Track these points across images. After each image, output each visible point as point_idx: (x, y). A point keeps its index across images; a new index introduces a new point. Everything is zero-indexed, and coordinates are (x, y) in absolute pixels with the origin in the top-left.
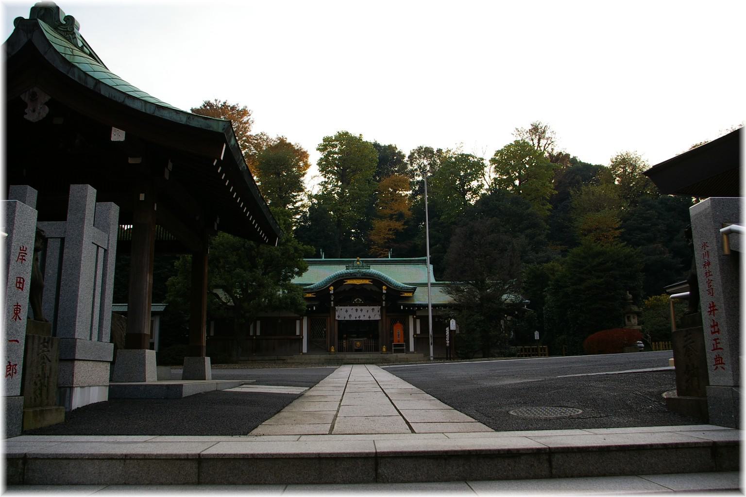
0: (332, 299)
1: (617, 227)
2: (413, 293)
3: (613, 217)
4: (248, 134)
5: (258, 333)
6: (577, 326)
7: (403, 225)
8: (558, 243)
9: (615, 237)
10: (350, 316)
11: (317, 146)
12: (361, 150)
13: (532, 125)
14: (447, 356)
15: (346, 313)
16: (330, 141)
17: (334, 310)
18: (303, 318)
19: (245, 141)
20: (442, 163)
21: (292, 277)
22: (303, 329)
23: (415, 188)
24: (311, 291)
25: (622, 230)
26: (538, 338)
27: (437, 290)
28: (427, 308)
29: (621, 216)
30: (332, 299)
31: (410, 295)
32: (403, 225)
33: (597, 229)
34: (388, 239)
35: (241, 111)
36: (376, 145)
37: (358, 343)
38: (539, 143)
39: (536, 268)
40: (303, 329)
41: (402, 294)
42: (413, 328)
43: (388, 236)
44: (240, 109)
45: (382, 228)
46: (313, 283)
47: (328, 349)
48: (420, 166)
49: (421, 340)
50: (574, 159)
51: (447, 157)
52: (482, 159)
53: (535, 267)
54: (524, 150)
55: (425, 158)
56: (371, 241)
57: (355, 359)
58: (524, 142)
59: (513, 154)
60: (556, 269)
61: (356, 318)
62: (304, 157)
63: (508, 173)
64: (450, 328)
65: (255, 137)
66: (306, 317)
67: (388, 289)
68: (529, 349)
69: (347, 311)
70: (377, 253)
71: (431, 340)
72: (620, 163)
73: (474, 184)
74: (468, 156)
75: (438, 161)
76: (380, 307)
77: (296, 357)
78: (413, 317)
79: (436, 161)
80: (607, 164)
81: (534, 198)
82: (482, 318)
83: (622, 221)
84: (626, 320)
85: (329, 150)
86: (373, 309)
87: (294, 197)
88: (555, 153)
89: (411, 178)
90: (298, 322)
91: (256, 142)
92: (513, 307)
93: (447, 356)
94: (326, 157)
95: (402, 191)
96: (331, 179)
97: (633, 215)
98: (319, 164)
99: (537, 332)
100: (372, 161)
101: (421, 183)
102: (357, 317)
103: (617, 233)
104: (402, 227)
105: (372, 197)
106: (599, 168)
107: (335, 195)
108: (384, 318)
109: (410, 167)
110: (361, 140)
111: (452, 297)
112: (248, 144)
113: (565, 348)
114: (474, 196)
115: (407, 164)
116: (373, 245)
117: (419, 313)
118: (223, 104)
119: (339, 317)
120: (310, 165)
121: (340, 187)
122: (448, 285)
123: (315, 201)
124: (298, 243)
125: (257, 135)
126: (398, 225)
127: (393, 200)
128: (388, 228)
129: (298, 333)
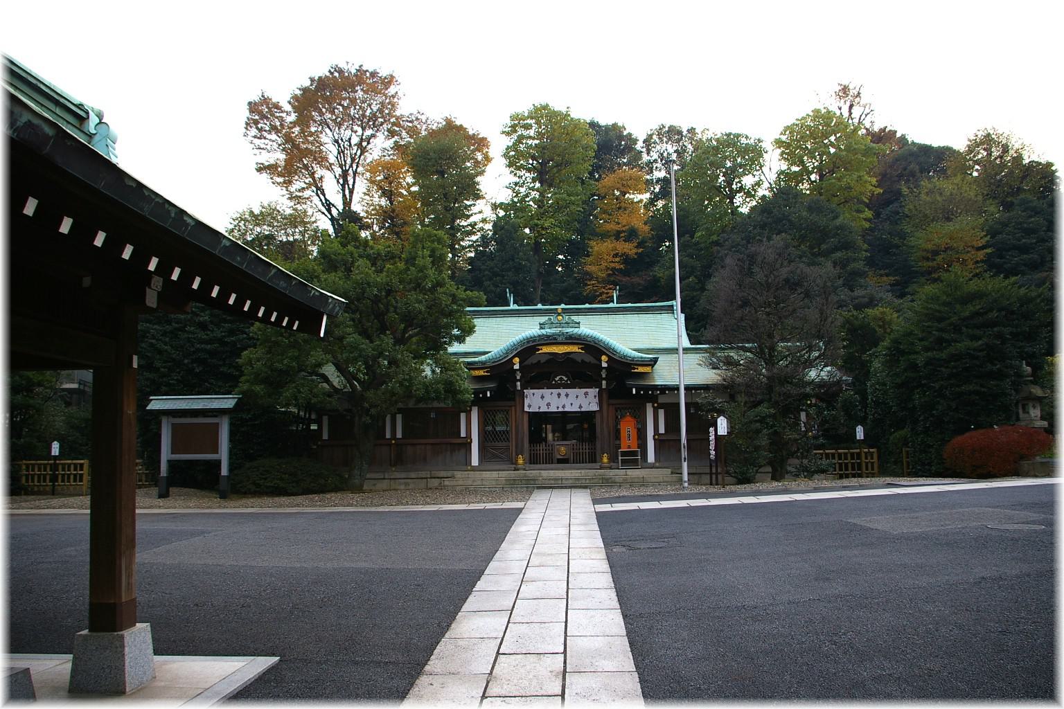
0: (518, 378)
1: (980, 245)
2: (653, 366)
3: (974, 230)
4: (398, 113)
5: (399, 435)
6: (931, 419)
7: (636, 247)
8: (882, 272)
9: (977, 262)
10: (548, 405)
11: (502, 128)
12: (569, 132)
13: (839, 84)
14: (711, 470)
15: (539, 400)
16: (520, 119)
17: (523, 396)
18: (471, 410)
19: (394, 124)
20: (696, 149)
21: (450, 344)
22: (472, 426)
23: (654, 189)
24: (482, 365)
25: (989, 251)
26: (862, 438)
27: (694, 358)
28: (676, 392)
29: (987, 228)
30: (518, 378)
31: (648, 369)
32: (636, 247)
33: (946, 249)
34: (613, 269)
35: (385, 78)
36: (593, 125)
37: (563, 449)
38: (851, 114)
39: (853, 316)
40: (472, 426)
41: (635, 369)
42: (654, 423)
43: (613, 265)
44: (384, 75)
45: (604, 252)
46: (487, 350)
47: (514, 461)
48: (662, 154)
49: (667, 444)
50: (903, 138)
51: (704, 140)
52: (760, 141)
53: (850, 314)
54: (828, 125)
55: (670, 142)
56: (587, 273)
57: (556, 479)
58: (829, 112)
59: (810, 131)
60: (888, 318)
61: (558, 408)
62: (484, 145)
63: (802, 163)
64: (716, 431)
65: (408, 117)
66: (477, 408)
67: (611, 360)
68: (845, 454)
69: (542, 397)
70: (596, 291)
71: (684, 453)
72: (982, 143)
73: (748, 181)
74: (738, 136)
75: (690, 146)
76: (598, 389)
77: (458, 474)
78: (653, 406)
79: (686, 147)
80: (960, 145)
81: (843, 200)
82: (772, 411)
83: (989, 236)
84: (1021, 411)
85: (520, 133)
86: (586, 394)
87: (467, 207)
88: (876, 129)
89: (648, 174)
90: (463, 416)
91: (410, 125)
92: (827, 392)
93: (711, 470)
94: (514, 147)
95: (633, 194)
96: (524, 178)
97: (1007, 226)
98: (506, 156)
99: (859, 427)
100: (586, 148)
101: (665, 182)
102: (560, 407)
103: (981, 255)
104: (635, 251)
105: (588, 204)
106: (944, 153)
107: (531, 203)
108: (605, 407)
109: (645, 158)
110: (569, 115)
111: (719, 375)
112: (397, 129)
113: (907, 452)
114: (748, 200)
115: (642, 152)
116: (590, 280)
117: (662, 400)
118: (358, 68)
119: (529, 406)
120: (492, 159)
121: (537, 190)
122: (705, 350)
123: (502, 213)
124: (456, 287)
125: (411, 114)
126: (629, 248)
127: (620, 208)
128: (612, 253)
129: (463, 434)
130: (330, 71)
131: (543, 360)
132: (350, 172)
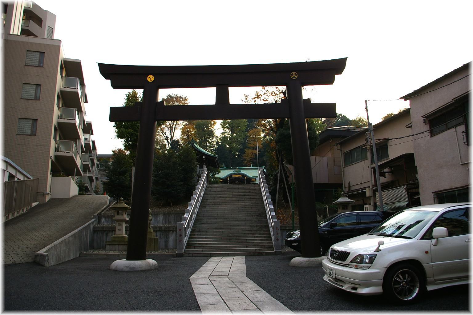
21: (216, 175)
24: (221, 179)
31: (254, 180)
34: (252, 158)
43: (252, 157)
67: (247, 178)
120: (216, 123)
130: (167, 96)
131: (234, 178)
132: (173, 127)
